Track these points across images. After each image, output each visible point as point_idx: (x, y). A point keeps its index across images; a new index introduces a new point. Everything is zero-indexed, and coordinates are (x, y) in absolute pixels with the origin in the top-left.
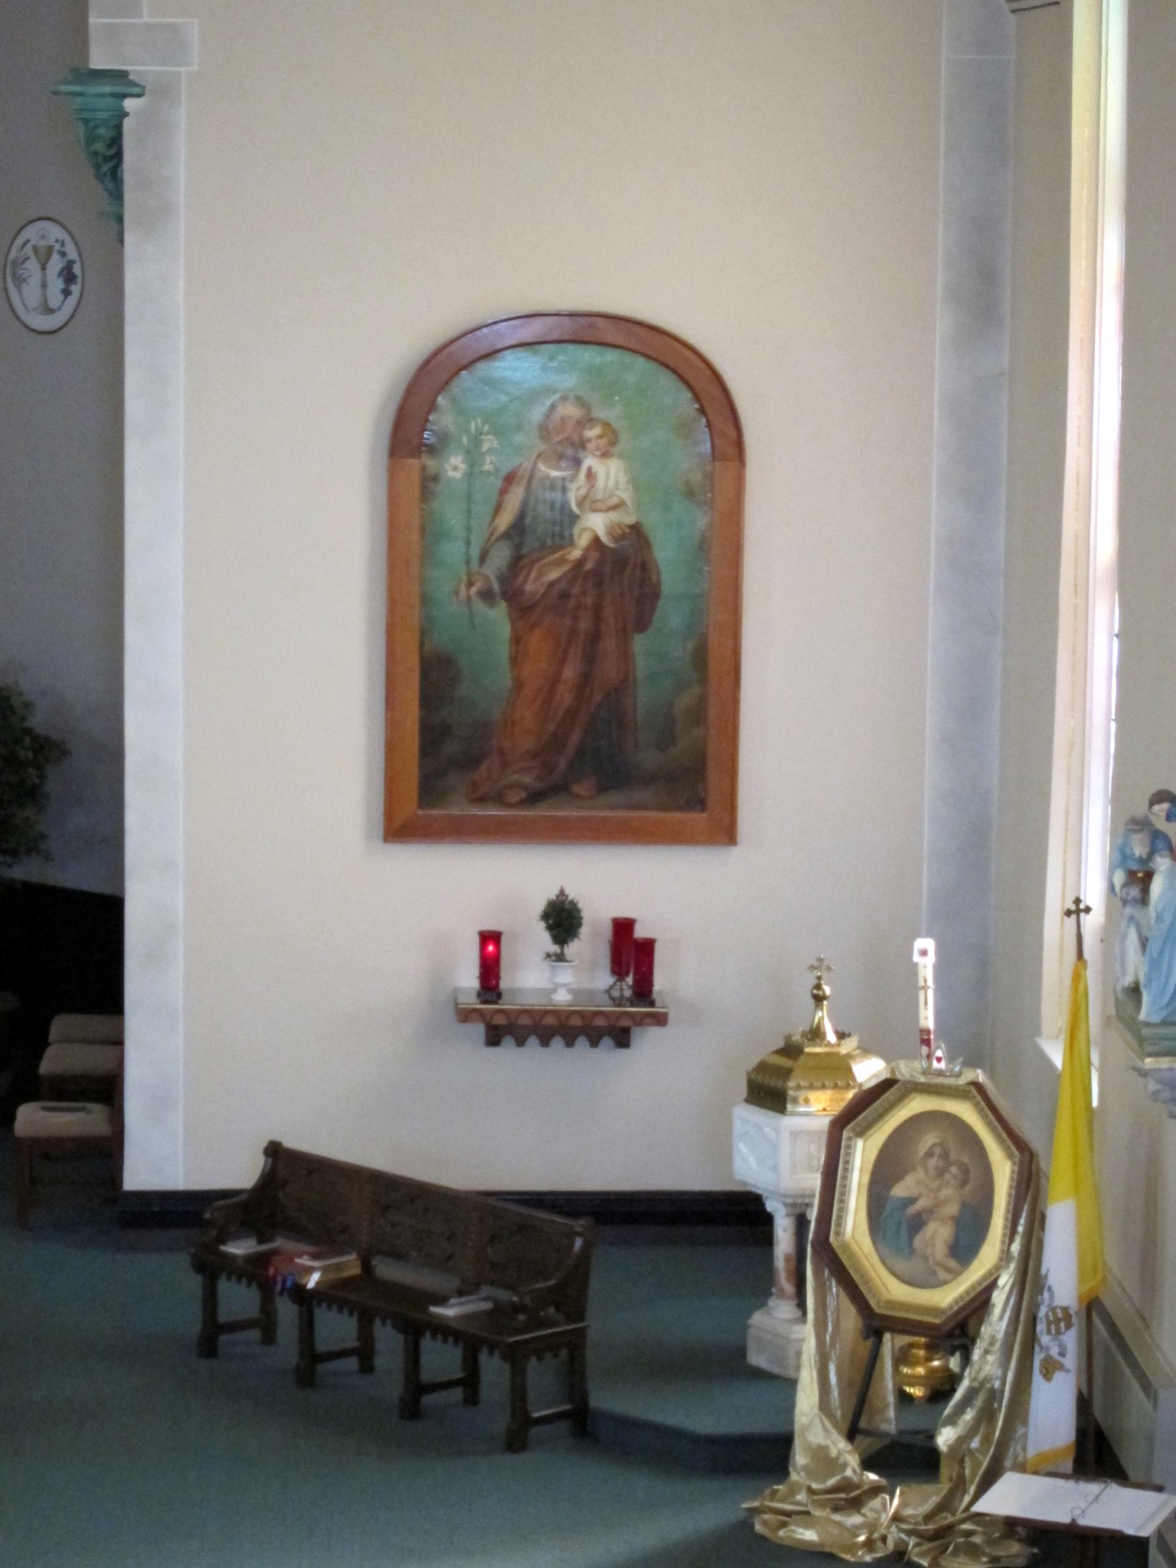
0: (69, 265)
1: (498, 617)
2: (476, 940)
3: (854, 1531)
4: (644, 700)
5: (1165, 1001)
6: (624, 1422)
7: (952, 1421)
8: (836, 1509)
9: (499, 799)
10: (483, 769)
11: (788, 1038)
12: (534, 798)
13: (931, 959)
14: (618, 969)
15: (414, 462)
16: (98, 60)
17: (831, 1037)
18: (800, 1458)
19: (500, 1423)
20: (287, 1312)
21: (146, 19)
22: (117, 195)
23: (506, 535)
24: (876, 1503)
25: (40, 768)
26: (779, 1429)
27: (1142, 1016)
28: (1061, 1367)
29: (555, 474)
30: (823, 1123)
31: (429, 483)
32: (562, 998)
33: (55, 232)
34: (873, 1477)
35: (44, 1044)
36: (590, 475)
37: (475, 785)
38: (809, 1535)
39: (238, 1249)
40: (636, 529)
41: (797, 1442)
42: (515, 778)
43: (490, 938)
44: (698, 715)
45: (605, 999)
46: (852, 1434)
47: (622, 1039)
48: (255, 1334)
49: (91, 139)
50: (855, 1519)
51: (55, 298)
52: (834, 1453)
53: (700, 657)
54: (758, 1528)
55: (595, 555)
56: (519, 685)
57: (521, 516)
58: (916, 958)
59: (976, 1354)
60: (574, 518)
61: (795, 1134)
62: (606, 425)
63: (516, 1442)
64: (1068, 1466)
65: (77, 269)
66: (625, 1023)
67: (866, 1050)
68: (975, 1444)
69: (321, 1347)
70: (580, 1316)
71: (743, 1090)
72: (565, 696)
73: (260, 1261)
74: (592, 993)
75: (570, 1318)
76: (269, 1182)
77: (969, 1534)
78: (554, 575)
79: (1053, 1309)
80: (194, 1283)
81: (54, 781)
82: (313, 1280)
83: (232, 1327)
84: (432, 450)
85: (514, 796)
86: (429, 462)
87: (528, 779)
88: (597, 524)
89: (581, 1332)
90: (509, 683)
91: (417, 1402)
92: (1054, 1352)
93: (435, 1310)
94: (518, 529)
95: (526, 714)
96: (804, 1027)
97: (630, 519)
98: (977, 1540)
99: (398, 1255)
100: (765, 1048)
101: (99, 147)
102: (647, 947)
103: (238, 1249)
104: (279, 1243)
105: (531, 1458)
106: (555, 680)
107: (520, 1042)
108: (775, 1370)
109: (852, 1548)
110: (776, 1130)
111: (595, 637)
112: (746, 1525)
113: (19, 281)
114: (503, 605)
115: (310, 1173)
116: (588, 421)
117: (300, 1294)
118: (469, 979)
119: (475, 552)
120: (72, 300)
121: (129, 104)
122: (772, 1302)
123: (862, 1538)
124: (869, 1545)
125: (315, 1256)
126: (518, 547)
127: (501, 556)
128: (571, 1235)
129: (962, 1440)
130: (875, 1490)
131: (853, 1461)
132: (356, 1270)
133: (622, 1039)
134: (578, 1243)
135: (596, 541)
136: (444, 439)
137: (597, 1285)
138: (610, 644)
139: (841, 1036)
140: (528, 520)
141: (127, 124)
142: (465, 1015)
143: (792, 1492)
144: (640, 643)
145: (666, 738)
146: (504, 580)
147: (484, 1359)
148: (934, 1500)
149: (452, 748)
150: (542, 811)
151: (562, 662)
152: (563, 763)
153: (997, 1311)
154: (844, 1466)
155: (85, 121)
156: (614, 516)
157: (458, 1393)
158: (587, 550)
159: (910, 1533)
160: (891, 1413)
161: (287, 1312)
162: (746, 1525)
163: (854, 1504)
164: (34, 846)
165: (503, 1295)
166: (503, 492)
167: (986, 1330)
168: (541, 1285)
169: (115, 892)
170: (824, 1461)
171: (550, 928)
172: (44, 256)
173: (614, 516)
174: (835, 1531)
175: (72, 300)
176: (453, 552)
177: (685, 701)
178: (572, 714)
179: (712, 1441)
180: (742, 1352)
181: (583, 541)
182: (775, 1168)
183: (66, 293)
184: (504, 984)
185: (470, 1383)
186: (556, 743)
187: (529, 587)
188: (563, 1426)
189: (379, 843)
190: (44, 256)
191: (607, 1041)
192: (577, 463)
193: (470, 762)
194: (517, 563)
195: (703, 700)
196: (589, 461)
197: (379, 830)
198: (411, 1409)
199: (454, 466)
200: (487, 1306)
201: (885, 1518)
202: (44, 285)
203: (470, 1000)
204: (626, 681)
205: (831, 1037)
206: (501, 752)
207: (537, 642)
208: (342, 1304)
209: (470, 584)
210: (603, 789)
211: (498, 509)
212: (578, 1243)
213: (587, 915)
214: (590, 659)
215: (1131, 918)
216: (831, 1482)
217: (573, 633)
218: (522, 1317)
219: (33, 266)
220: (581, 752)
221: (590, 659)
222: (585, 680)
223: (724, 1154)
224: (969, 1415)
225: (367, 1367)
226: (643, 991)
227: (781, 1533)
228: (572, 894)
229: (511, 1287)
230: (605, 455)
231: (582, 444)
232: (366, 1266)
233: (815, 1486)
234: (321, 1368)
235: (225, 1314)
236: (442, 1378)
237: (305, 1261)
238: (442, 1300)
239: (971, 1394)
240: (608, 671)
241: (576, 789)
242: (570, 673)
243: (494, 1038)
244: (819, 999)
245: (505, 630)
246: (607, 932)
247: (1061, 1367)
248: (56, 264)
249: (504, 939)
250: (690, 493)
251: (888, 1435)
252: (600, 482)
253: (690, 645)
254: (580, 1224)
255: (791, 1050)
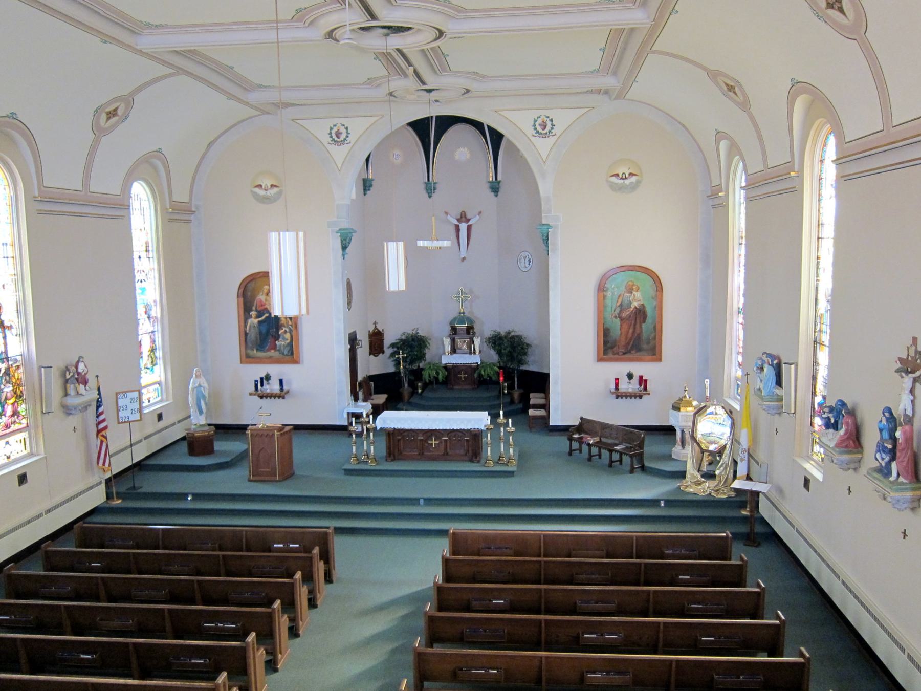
0: (530, 260)
1: (618, 320)
2: (614, 380)
3: (700, 489)
4: (644, 336)
5: (767, 391)
6: (651, 468)
7: (719, 469)
8: (696, 485)
9: (618, 354)
10: (615, 349)
11: (680, 398)
12: (624, 354)
13: (708, 383)
14: (640, 384)
15: (602, 294)
16: (544, 222)
17: (688, 397)
18: (688, 475)
19: (629, 468)
20: (585, 448)
21: (552, 214)
22: (547, 246)
23: (619, 306)
24: (704, 484)
25: (527, 349)
26: (685, 470)
27: (763, 394)
28: (744, 460)
29: (628, 295)
30: (692, 413)
31: (605, 297)
32: (630, 390)
33: (527, 254)
34: (703, 479)
35: (530, 399)
36: (634, 295)
37: (613, 352)
38: (691, 490)
39: (576, 436)
40: (643, 305)
41: (688, 472)
42: (620, 350)
43: (617, 379)
44: (655, 338)
45: (637, 390)
46: (699, 471)
47: (641, 397)
48: (578, 451)
49: (543, 236)
50: (700, 487)
51: (527, 265)
52: (695, 475)
53: (655, 328)
54: (681, 488)
55: (635, 309)
56: (621, 334)
57: (622, 303)
58: (705, 383)
59: (723, 457)
60: (631, 303)
61: (682, 415)
62: (637, 286)
63: (632, 471)
64: (745, 479)
65: (531, 260)
66: (642, 394)
67: (694, 400)
68: (723, 473)
69: (592, 454)
70: (643, 449)
71: (671, 407)
72: (630, 335)
73: (581, 438)
74: (635, 389)
75: (641, 449)
76: (581, 424)
77: (723, 490)
78: (628, 313)
79: (743, 449)
80: (568, 442)
81: (530, 351)
82: (591, 442)
83: (574, 450)
84: (605, 291)
85: (621, 354)
86: (604, 293)
87: (623, 350)
88: (635, 304)
89: (643, 452)
90: (619, 333)
91: (611, 464)
92: (743, 457)
93: (615, 447)
94: (621, 305)
95: (623, 339)
96: (683, 396)
97: (642, 303)
98: (725, 491)
99: (606, 437)
100: (675, 399)
101: (544, 238)
102: (646, 381)
103: (576, 436)
104: (582, 435)
105: (635, 475)
106: (628, 332)
107: (622, 398)
108: (677, 459)
109: (701, 493)
110: (678, 414)
111: (635, 325)
112: (679, 488)
113: (520, 263)
114: (618, 319)
115: (589, 422)
116: (633, 285)
117: (589, 445)
118: (613, 387)
119: (613, 309)
120: (530, 265)
121: (549, 230)
122: (676, 446)
123: (702, 491)
124: (704, 492)
125: (592, 437)
126: (621, 308)
127: (618, 310)
128: (641, 434)
129: (721, 473)
130: (704, 482)
131: (700, 476)
132: (599, 440)
133: (641, 397)
134: (642, 436)
135: (636, 307)
136: (608, 289)
137: (646, 443)
138: (638, 326)
139: (690, 397)
140: (623, 303)
141: (549, 233)
142: (613, 393)
143: (686, 482)
144: (644, 326)
145: (648, 343)
146: (619, 314)
147: (602, 450)
148: (716, 484)
149: (609, 345)
150: (626, 356)
151: (630, 328)
152: (629, 347)
153: (727, 449)
154: (698, 477)
155: (542, 233)
156: (639, 302)
157: (618, 463)
158: (634, 308)
159: (712, 490)
160: (705, 467)
161: (585, 448)
162: (679, 488)
163: (700, 484)
164: (525, 363)
165: (628, 445)
166: (618, 298)
167: (725, 452)
168: (636, 443)
169: (545, 371)
170: (693, 476)
171: (628, 377)
172: (525, 259)
173: (639, 302)
174: (696, 489)
175: (530, 265)
176: (609, 309)
177: (653, 335)
178: (631, 339)
179: (669, 472)
180: (671, 456)
181: (633, 307)
182: (678, 422)
183: (529, 264)
184: (619, 388)
185: (621, 461)
186: (628, 343)
187: (623, 315)
188: (639, 469)
189: (597, 363)
190: (525, 259)
191: (638, 398)
192: (632, 293)
193: (612, 348)
194: (621, 311)
195: (655, 336)
196: (634, 293)
197: (596, 360)
198: (610, 466)
199: (609, 294)
200: (624, 447)
201: (706, 487)
202: (525, 263)
203: (613, 391)
204: (641, 332)
205: (688, 397)
206: (618, 346)
207: (625, 326)
208: (595, 446)
209: (612, 315)
210: (637, 352)
211: (618, 301)
212: (642, 436)
213: (634, 374)
214: (635, 328)
215: (758, 376)
216: (695, 480)
217: (631, 323)
218: (633, 449)
219: (523, 260)
220: (633, 345)
221: (635, 328)
222: (634, 332)
223: (668, 420)
224: (722, 468)
225: (581, 452)
226: (645, 389)
227: (686, 489)
228: (632, 371)
229: (630, 444)
230: (637, 291)
231: (633, 289)
232: (600, 439)
233: (692, 481)
234: (613, 464)
235: (573, 448)
236: (594, 454)
237: (590, 438)
238: (617, 445)
239: (723, 464)
240: (638, 331)
241: (632, 352)
242: (631, 331)
243: (617, 397)
244: (685, 390)
245: (619, 323)
246: (638, 378)
247: (744, 460)
248: (527, 259)
249: (619, 380)
250: (653, 298)
251: (704, 471)
252: (636, 296)
253: (653, 326)
254: (642, 432)
255: (681, 400)
